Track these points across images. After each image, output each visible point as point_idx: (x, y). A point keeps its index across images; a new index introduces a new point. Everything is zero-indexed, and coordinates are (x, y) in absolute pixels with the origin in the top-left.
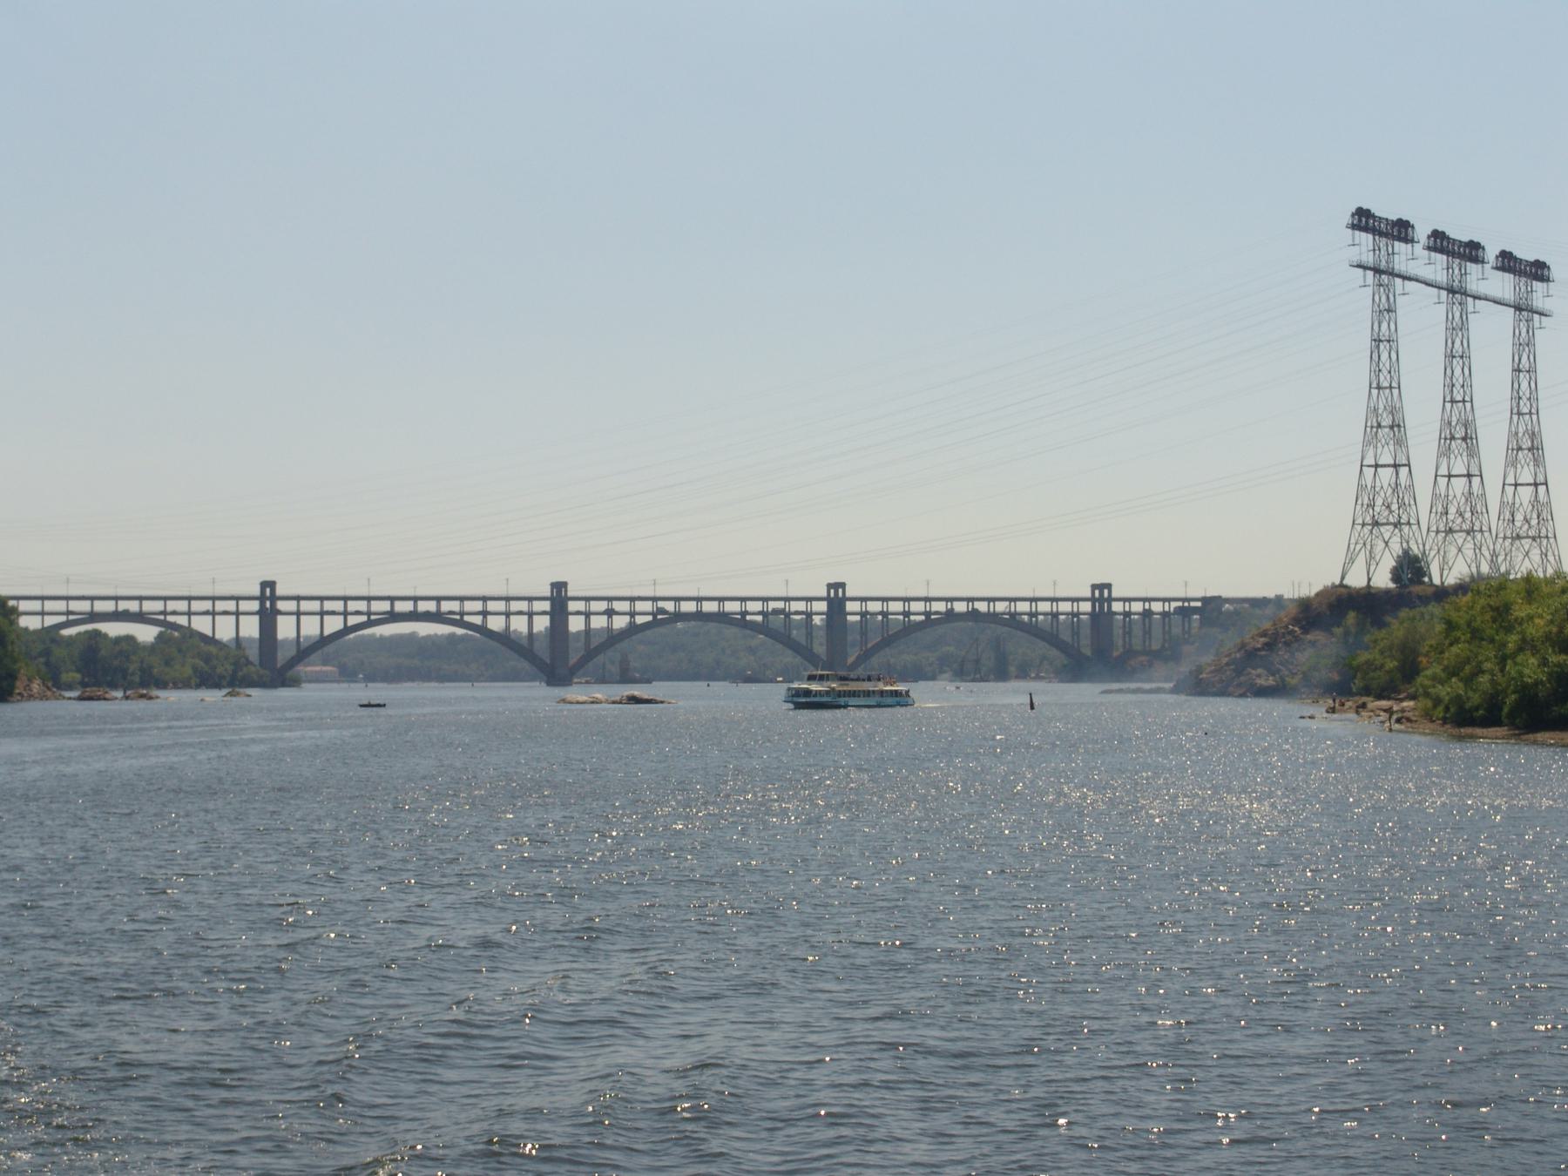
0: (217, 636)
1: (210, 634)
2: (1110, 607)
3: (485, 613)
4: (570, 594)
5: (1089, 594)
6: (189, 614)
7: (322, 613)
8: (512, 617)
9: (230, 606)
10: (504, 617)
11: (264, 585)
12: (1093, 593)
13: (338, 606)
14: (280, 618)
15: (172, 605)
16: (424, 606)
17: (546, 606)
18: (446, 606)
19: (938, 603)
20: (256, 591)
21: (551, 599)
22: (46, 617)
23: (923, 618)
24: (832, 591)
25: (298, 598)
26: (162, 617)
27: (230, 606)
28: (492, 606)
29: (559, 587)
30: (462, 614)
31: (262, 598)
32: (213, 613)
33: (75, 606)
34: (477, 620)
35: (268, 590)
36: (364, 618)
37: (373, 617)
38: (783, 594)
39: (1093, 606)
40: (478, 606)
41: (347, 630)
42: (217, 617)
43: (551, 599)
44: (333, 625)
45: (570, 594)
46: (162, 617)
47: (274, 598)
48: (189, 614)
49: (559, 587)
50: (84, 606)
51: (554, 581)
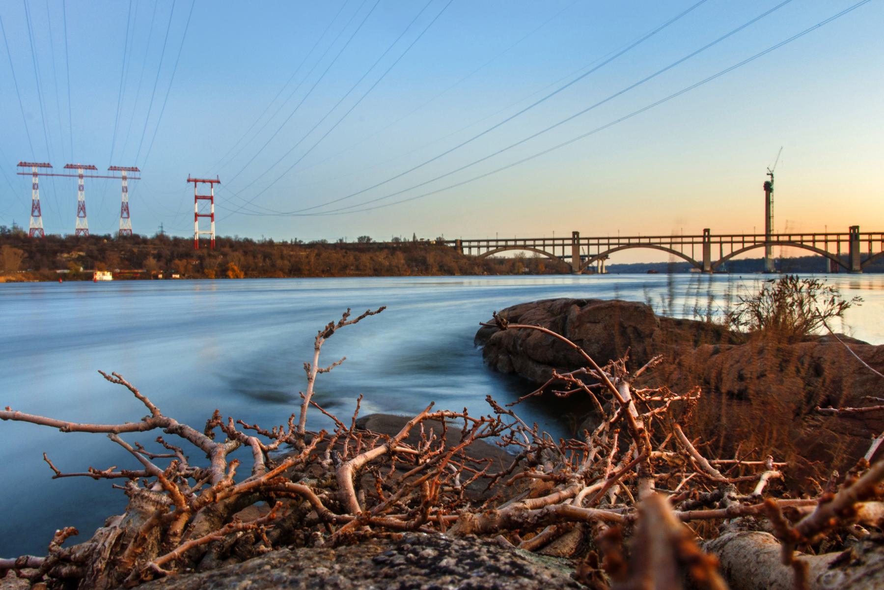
0: (829, 251)
1: (691, 257)
2: (709, 239)
3: (814, 241)
4: (860, 231)
5: (702, 234)
6: (544, 246)
7: (588, 245)
8: (472, 249)
9: (560, 242)
10: (867, 243)
11: (706, 230)
12: (850, 231)
13: (485, 244)
14: (712, 245)
15: (805, 238)
16: (519, 243)
17: (847, 237)
18: (528, 243)
19: (819, 243)
20: (571, 236)
21: (850, 234)
22: (734, 244)
23: (495, 248)
24: (852, 231)
25: (588, 239)
26: (659, 245)
27: (560, 242)
28: (547, 242)
29: (854, 228)
30: (802, 241)
31: (573, 239)
32: (693, 243)
33: (622, 241)
34: (811, 244)
35: (576, 236)
36: (753, 244)
37: (756, 244)
38: (753, 233)
39: (704, 239)
40: (541, 242)
41: (489, 253)
42: (565, 247)
43: (850, 234)
44: (483, 251)
45: (860, 231)
46: (659, 245)
47: (579, 239)
48: (544, 246)
49: (575, 233)
50: (626, 241)
51: (851, 226)
